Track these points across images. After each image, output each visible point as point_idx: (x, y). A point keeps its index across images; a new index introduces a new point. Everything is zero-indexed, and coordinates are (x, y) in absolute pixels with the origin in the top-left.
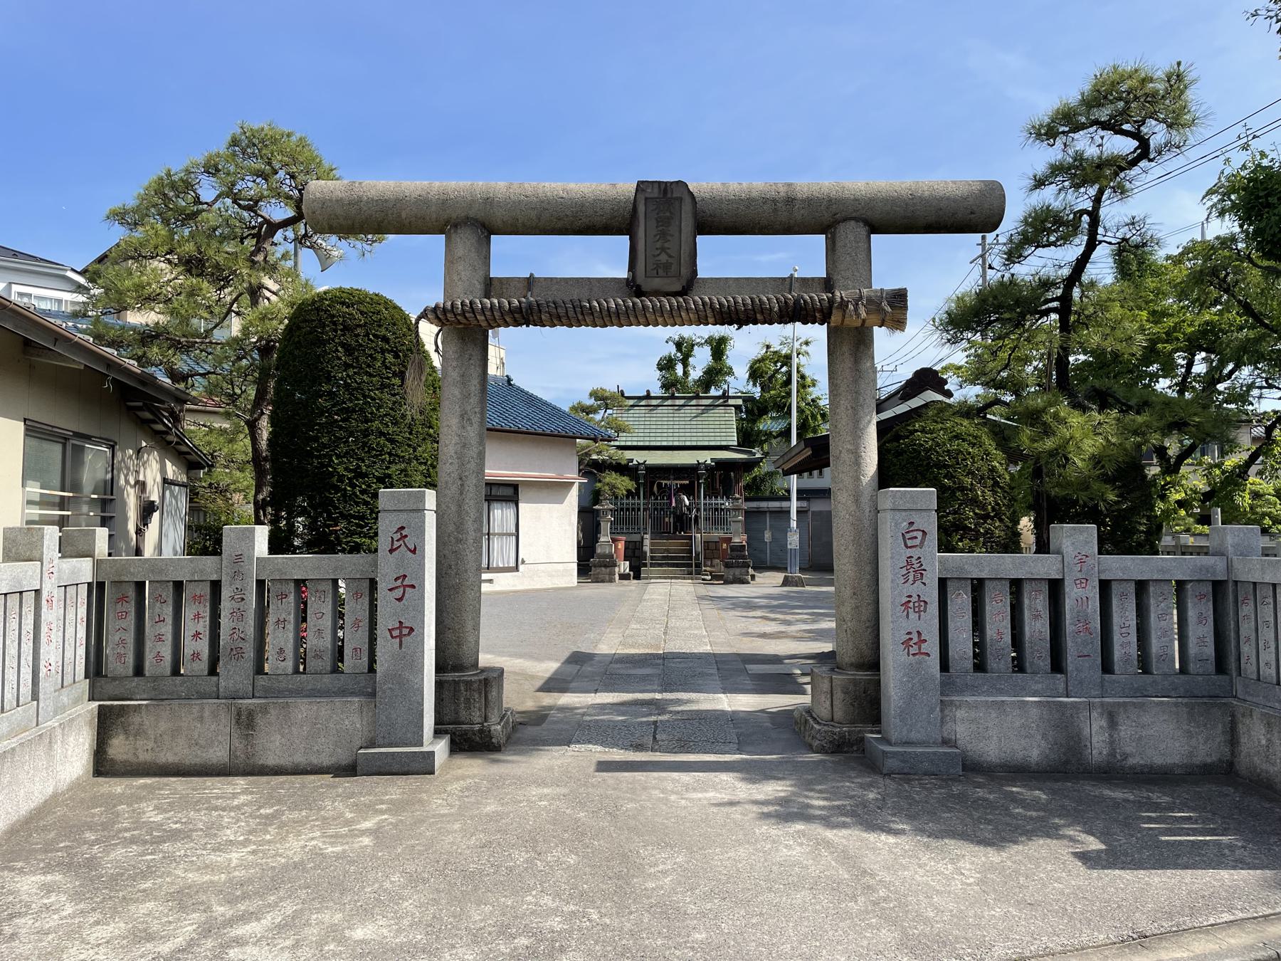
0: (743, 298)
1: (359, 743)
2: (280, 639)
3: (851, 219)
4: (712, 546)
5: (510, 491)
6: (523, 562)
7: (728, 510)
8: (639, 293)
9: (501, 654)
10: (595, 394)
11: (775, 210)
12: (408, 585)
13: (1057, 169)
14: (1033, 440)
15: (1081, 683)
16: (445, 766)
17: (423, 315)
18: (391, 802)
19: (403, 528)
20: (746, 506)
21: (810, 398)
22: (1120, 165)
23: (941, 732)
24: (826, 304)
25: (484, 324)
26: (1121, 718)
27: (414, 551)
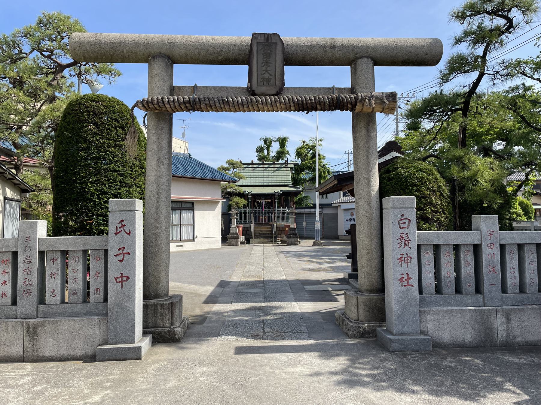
0: (310, 97)
1: (98, 342)
2: (53, 284)
3: (365, 57)
4: (281, 229)
5: (190, 205)
6: (197, 237)
7: (288, 213)
8: (254, 94)
9: (184, 282)
10: (228, 162)
11: (325, 52)
12: (125, 253)
13: (467, 34)
14: (459, 172)
15: (491, 299)
16: (149, 353)
17: (136, 105)
18: (113, 380)
19: (123, 221)
20: (296, 211)
21: (322, 164)
22: (499, 32)
23: (420, 327)
24: (353, 99)
25: (169, 110)
26: (512, 317)
27: (129, 234)
